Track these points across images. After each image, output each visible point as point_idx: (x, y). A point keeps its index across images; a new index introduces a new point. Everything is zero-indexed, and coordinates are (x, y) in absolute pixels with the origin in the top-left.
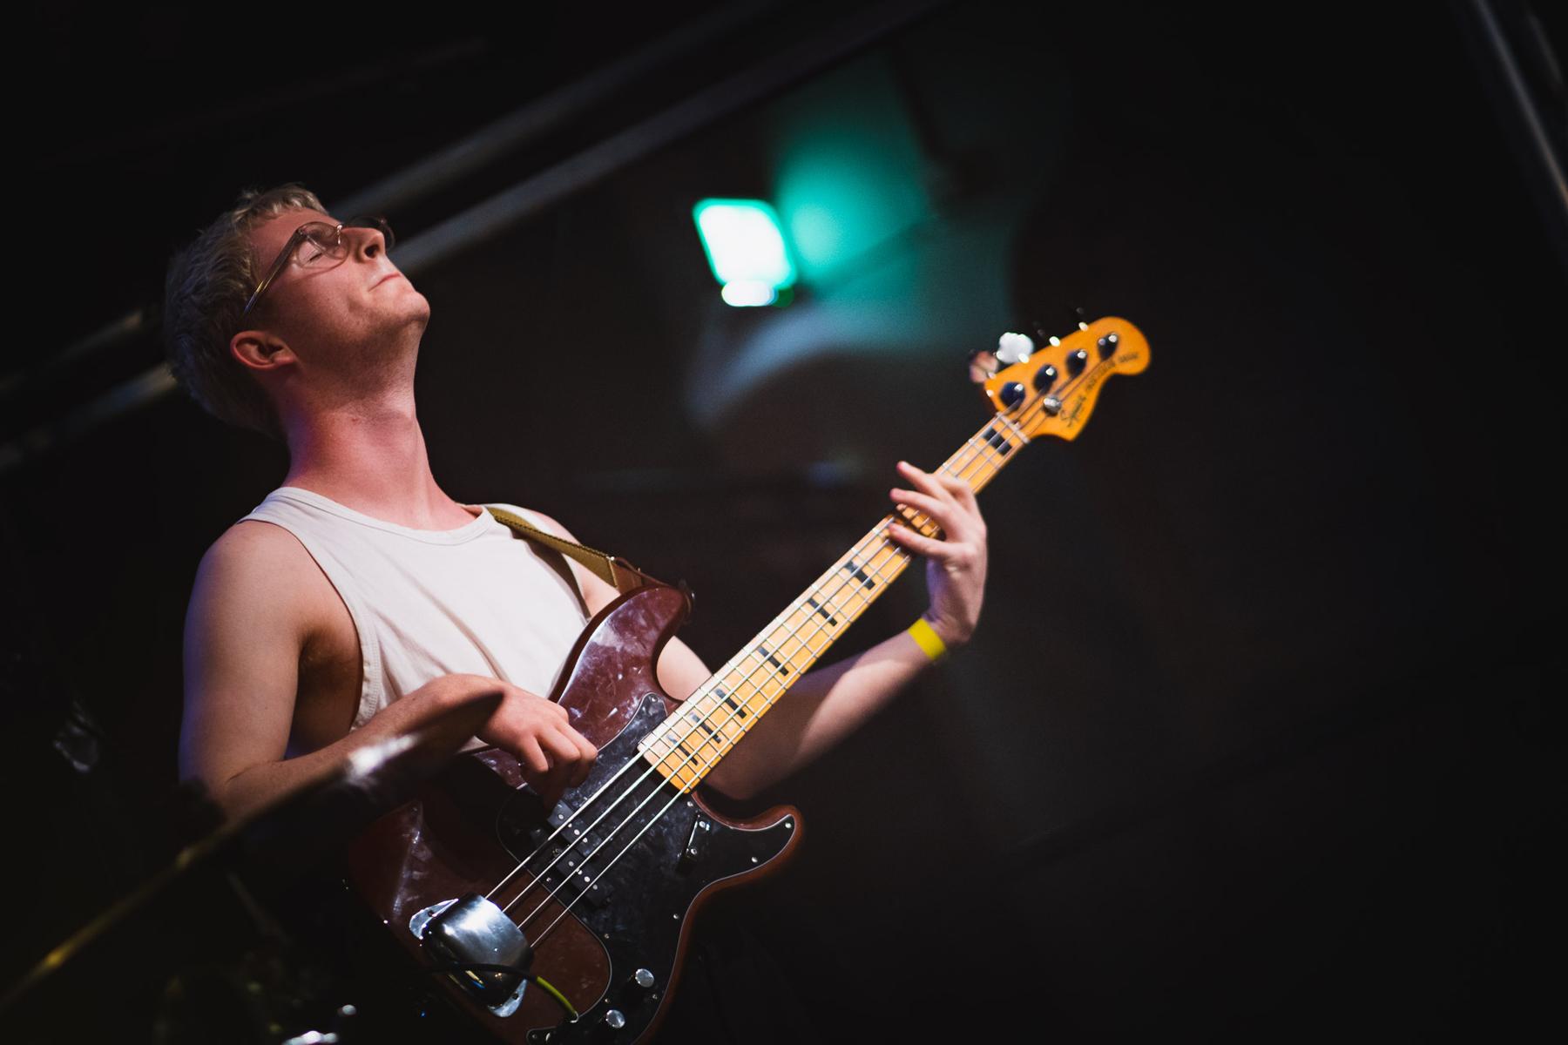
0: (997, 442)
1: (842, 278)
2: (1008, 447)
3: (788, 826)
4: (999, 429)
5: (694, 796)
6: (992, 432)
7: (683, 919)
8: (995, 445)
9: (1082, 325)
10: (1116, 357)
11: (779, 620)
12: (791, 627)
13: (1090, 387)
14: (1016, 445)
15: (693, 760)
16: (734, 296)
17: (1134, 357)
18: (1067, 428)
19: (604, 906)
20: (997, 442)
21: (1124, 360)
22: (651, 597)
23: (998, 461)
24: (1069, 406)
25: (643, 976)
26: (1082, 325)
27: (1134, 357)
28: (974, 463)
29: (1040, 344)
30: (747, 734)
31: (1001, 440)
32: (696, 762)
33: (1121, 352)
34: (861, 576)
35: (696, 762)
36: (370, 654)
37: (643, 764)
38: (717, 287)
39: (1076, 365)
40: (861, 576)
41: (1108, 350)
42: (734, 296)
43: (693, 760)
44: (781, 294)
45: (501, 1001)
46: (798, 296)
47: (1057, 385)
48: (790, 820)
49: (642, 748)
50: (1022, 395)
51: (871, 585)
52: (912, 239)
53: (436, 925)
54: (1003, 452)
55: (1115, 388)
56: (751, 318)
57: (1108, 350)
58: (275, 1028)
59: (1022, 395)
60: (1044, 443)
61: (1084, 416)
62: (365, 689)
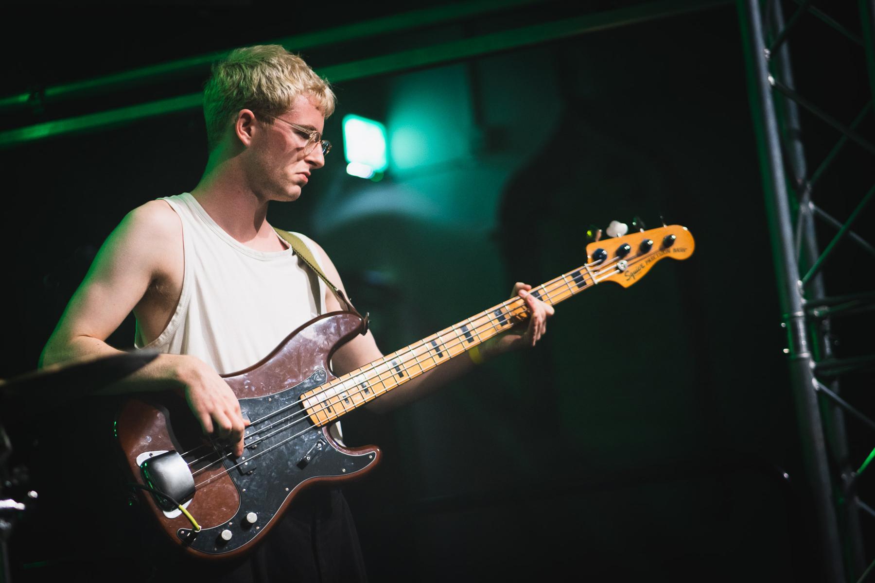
0: (579, 280)
1: (411, 175)
2: (585, 284)
3: (371, 457)
4: (583, 272)
5: (324, 429)
6: (578, 273)
7: (290, 493)
8: (576, 281)
9: (642, 230)
10: (671, 249)
11: (411, 347)
12: (415, 353)
13: (649, 261)
14: (589, 283)
15: (328, 408)
16: (351, 170)
17: (683, 250)
18: (626, 282)
19: (248, 474)
20: (579, 280)
21: (675, 251)
22: (343, 318)
23: (574, 289)
24: (632, 269)
25: (252, 517)
26: (642, 230)
27: (683, 250)
28: (561, 288)
29: (632, 230)
30: (366, 404)
31: (582, 278)
32: (330, 411)
33: (676, 245)
34: (467, 334)
35: (330, 411)
36: (183, 300)
37: (301, 405)
38: (345, 163)
39: (645, 248)
40: (467, 334)
41: (668, 242)
42: (351, 170)
43: (328, 408)
44: (377, 174)
45: (169, 509)
46: (386, 178)
47: (630, 256)
48: (373, 455)
49: (303, 397)
50: (604, 257)
51: (432, 341)
52: (455, 165)
53: (151, 461)
54: (579, 286)
55: (666, 266)
56: (358, 183)
57: (668, 242)
58: (287, 489)
59: (604, 257)
60: (609, 286)
61: (638, 277)
62: (174, 317)
